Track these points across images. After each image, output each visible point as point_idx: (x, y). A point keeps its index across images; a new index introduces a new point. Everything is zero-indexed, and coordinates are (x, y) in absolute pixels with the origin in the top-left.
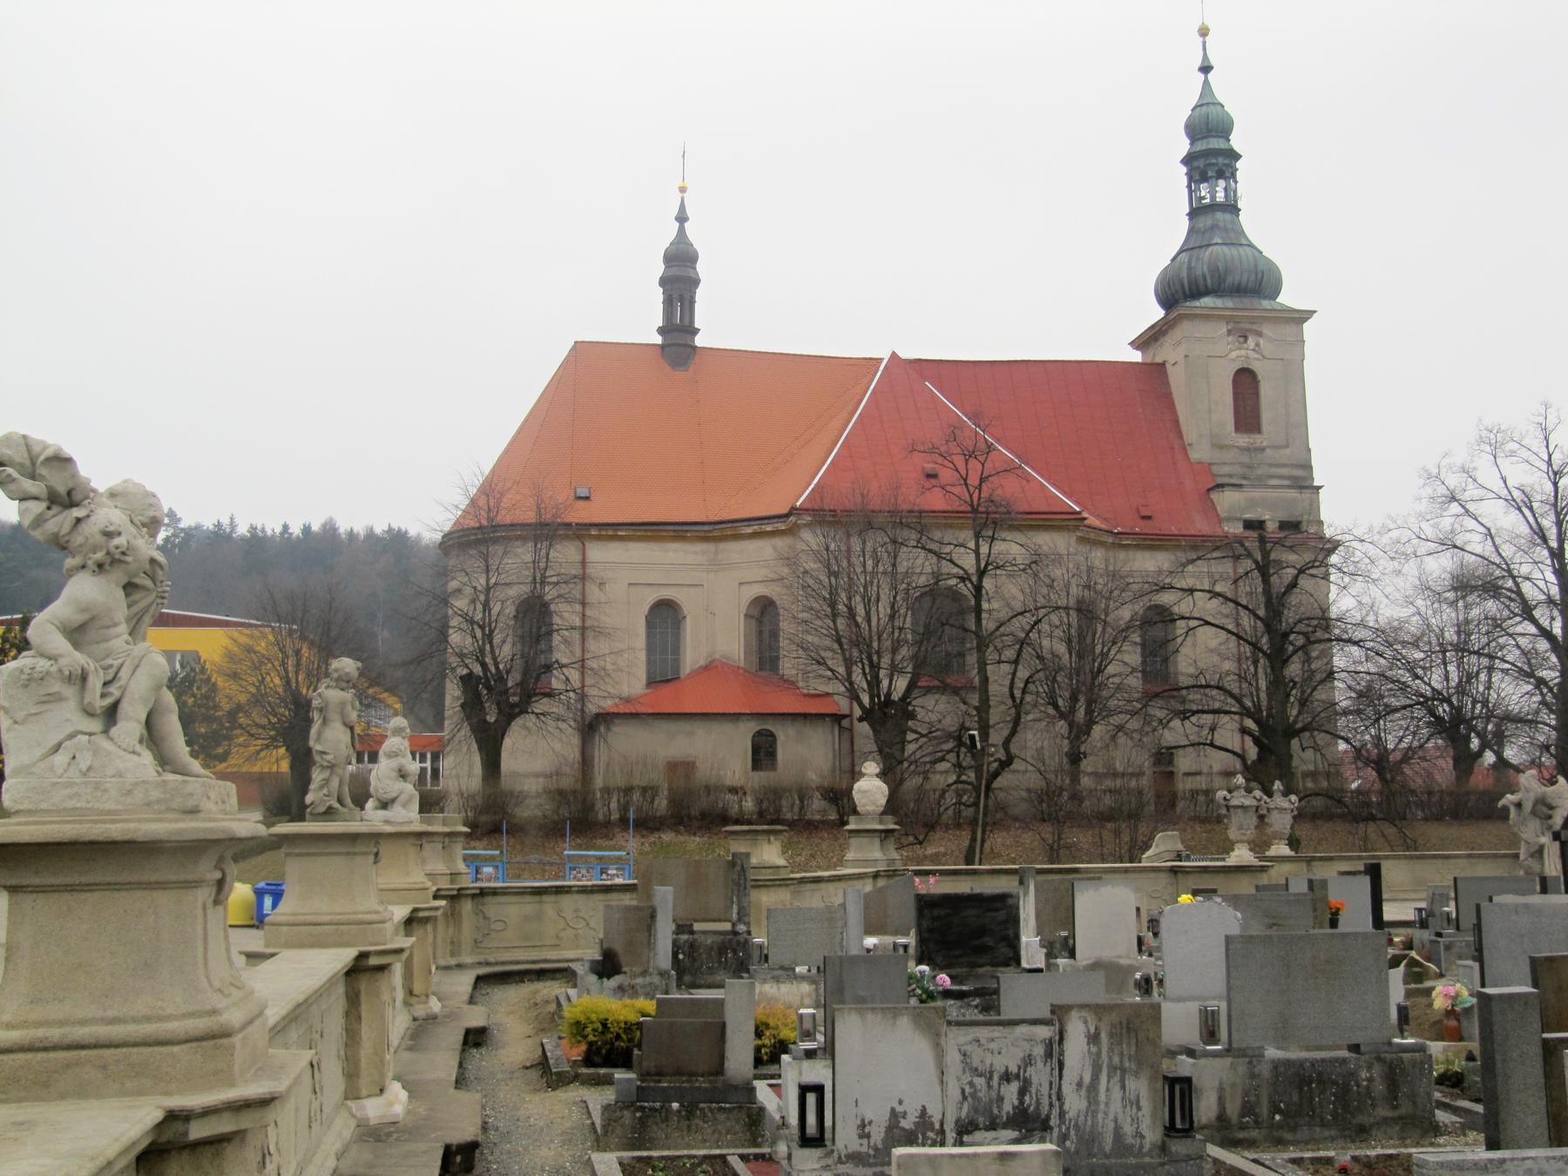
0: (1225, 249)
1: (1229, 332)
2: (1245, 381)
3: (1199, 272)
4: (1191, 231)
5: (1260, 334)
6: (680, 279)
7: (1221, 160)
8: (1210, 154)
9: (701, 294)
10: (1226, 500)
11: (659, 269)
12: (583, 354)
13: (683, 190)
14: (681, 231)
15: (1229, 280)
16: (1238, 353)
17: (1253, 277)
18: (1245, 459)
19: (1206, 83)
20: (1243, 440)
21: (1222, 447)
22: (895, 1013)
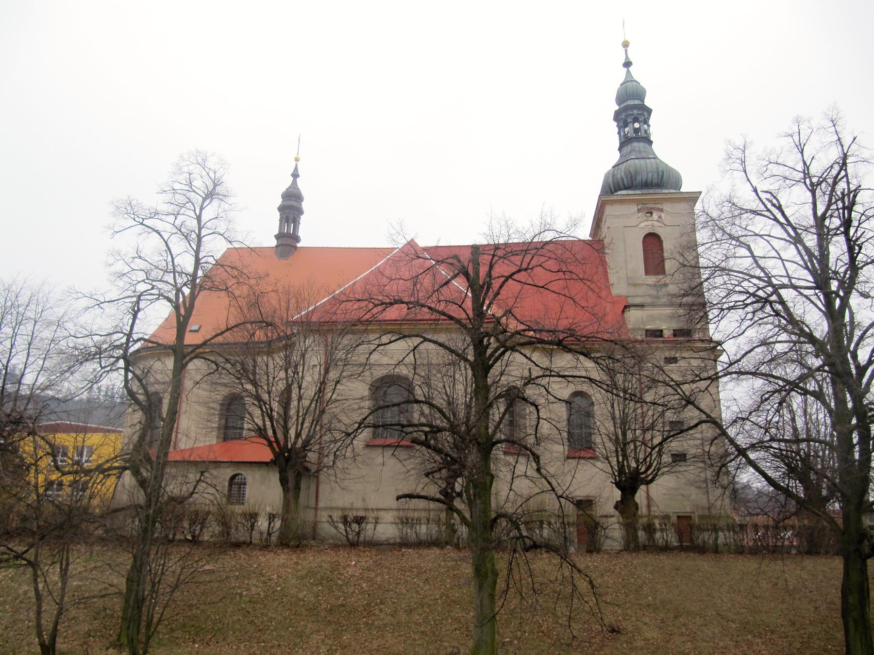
0: (637, 161)
1: (639, 211)
2: (652, 241)
3: (619, 176)
4: (621, 157)
5: (662, 210)
6: (291, 207)
7: (635, 112)
8: (632, 113)
9: (303, 219)
10: (633, 315)
11: (279, 201)
13: (297, 160)
14: (294, 183)
15: (639, 178)
16: (646, 223)
17: (655, 176)
18: (654, 292)
20: (652, 279)
21: (635, 285)
22: (157, 368)
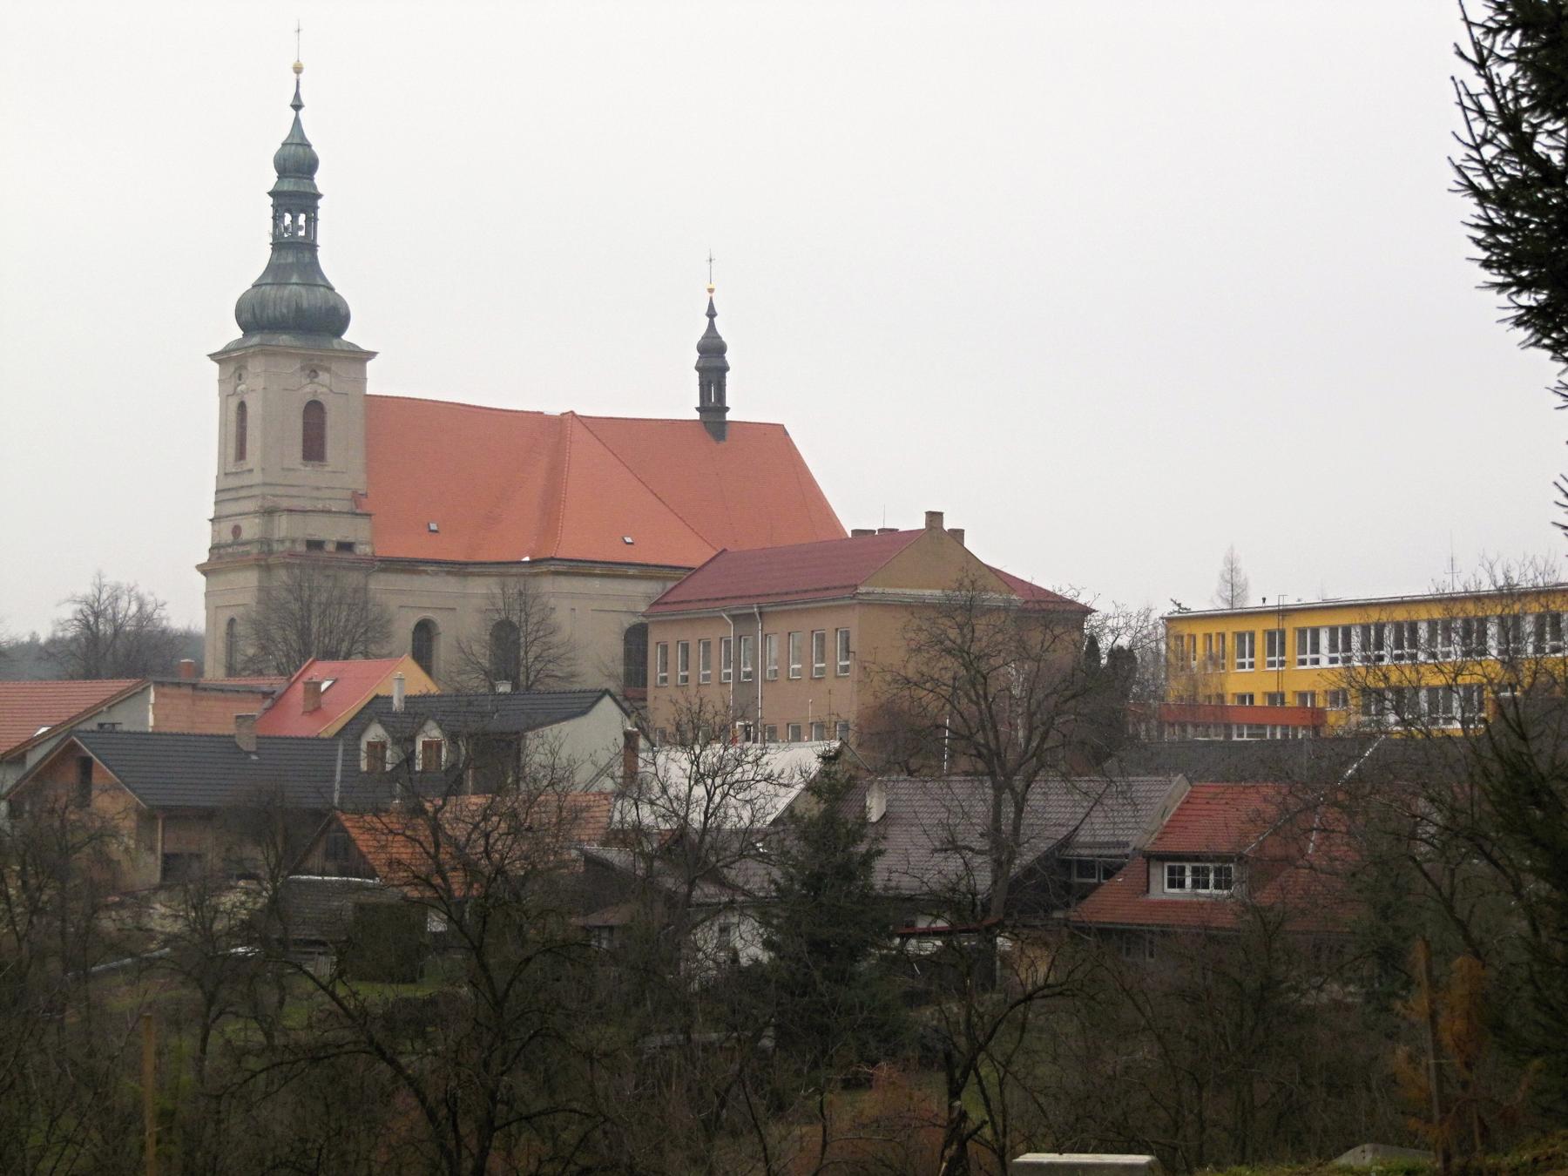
1: (302, 369)
6: (712, 362)
12: (779, 431)
14: (712, 326)
19: (297, 121)
